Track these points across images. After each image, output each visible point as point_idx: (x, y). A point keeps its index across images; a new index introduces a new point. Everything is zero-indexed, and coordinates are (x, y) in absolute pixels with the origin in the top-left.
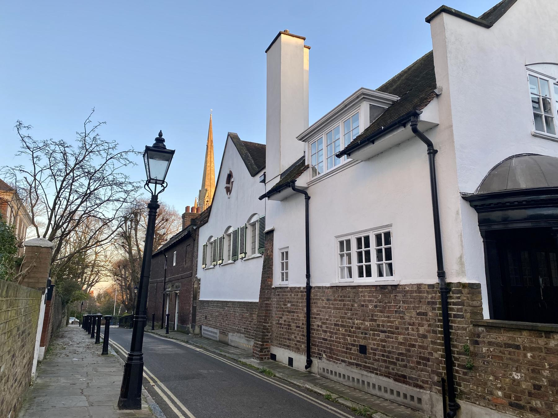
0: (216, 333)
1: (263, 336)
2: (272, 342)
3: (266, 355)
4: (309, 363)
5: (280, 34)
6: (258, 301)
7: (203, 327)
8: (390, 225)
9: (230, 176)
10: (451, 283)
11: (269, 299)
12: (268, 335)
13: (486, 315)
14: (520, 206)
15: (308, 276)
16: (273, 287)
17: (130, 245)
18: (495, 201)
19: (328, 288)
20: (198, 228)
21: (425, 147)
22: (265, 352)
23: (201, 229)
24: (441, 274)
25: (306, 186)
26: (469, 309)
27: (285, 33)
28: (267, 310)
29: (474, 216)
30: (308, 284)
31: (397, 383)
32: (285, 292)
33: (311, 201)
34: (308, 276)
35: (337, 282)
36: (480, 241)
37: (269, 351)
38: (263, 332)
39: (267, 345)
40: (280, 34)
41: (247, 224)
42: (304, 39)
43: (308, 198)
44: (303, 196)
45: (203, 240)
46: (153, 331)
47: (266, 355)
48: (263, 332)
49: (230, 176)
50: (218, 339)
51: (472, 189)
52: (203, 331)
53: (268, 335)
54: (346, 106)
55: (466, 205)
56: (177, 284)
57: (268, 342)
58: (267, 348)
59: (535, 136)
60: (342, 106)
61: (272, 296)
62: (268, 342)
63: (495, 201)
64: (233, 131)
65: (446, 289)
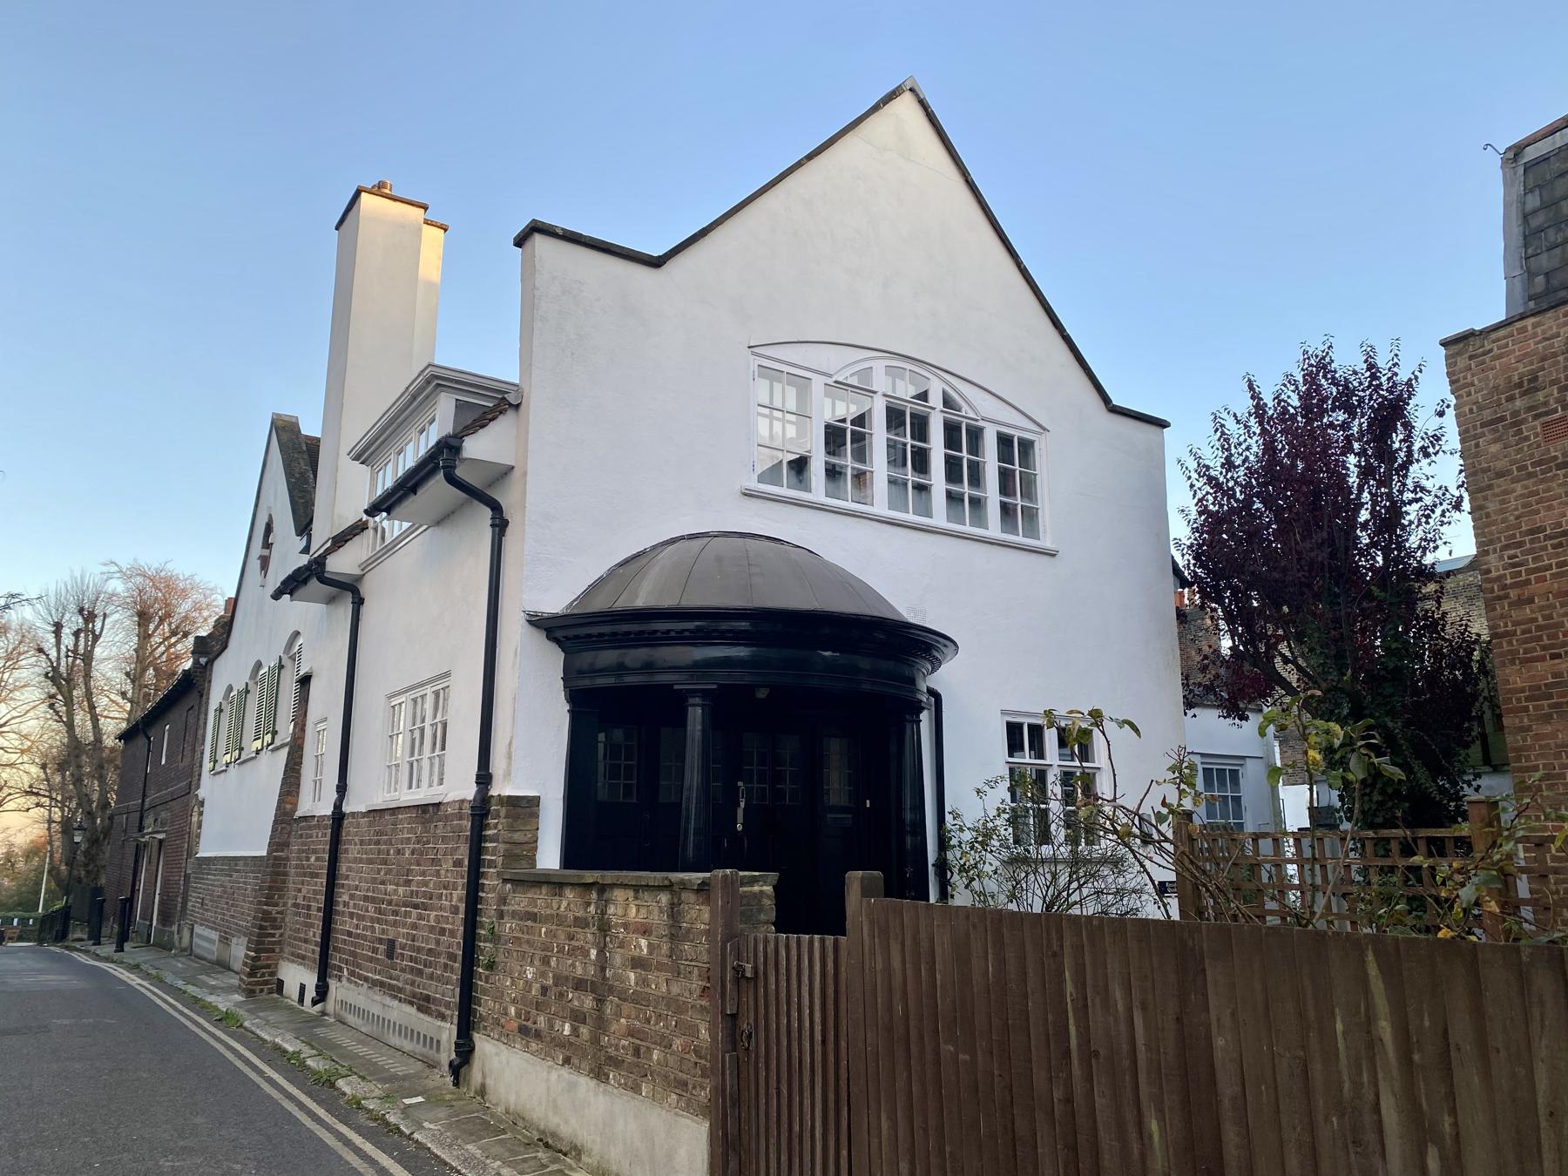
0: (211, 941)
1: (259, 935)
2: (282, 950)
3: (266, 983)
4: (322, 993)
5: (358, 193)
6: (264, 853)
7: (198, 929)
8: (447, 675)
9: (269, 529)
10: (1311, 809)
11: (287, 845)
12: (273, 935)
13: (549, 856)
14: (682, 639)
15: (342, 788)
16: (298, 814)
17: (69, 702)
18: (634, 627)
19: (364, 815)
20: (211, 662)
21: (488, 512)
22: (263, 975)
23: (217, 663)
24: (484, 778)
25: (357, 572)
26: (502, 847)
27: (379, 190)
28: (278, 874)
29: (553, 660)
30: (338, 806)
31: (421, 1015)
32: (310, 828)
33: (365, 609)
34: (342, 788)
35: (380, 801)
36: (564, 708)
37: (273, 974)
38: (261, 928)
39: (268, 958)
40: (358, 193)
41: (285, 658)
42: (425, 208)
43: (359, 602)
44: (349, 598)
45: (216, 697)
46: (117, 956)
47: (266, 983)
48: (261, 928)
49: (269, 529)
50: (214, 957)
51: (555, 603)
52: (195, 940)
53: (273, 935)
54: (414, 397)
55: (539, 637)
56: (163, 815)
57: (273, 951)
58: (268, 966)
59: (749, 494)
60: (407, 397)
61: (293, 840)
62: (273, 951)
63: (634, 627)
64: (287, 410)
65: (482, 808)
